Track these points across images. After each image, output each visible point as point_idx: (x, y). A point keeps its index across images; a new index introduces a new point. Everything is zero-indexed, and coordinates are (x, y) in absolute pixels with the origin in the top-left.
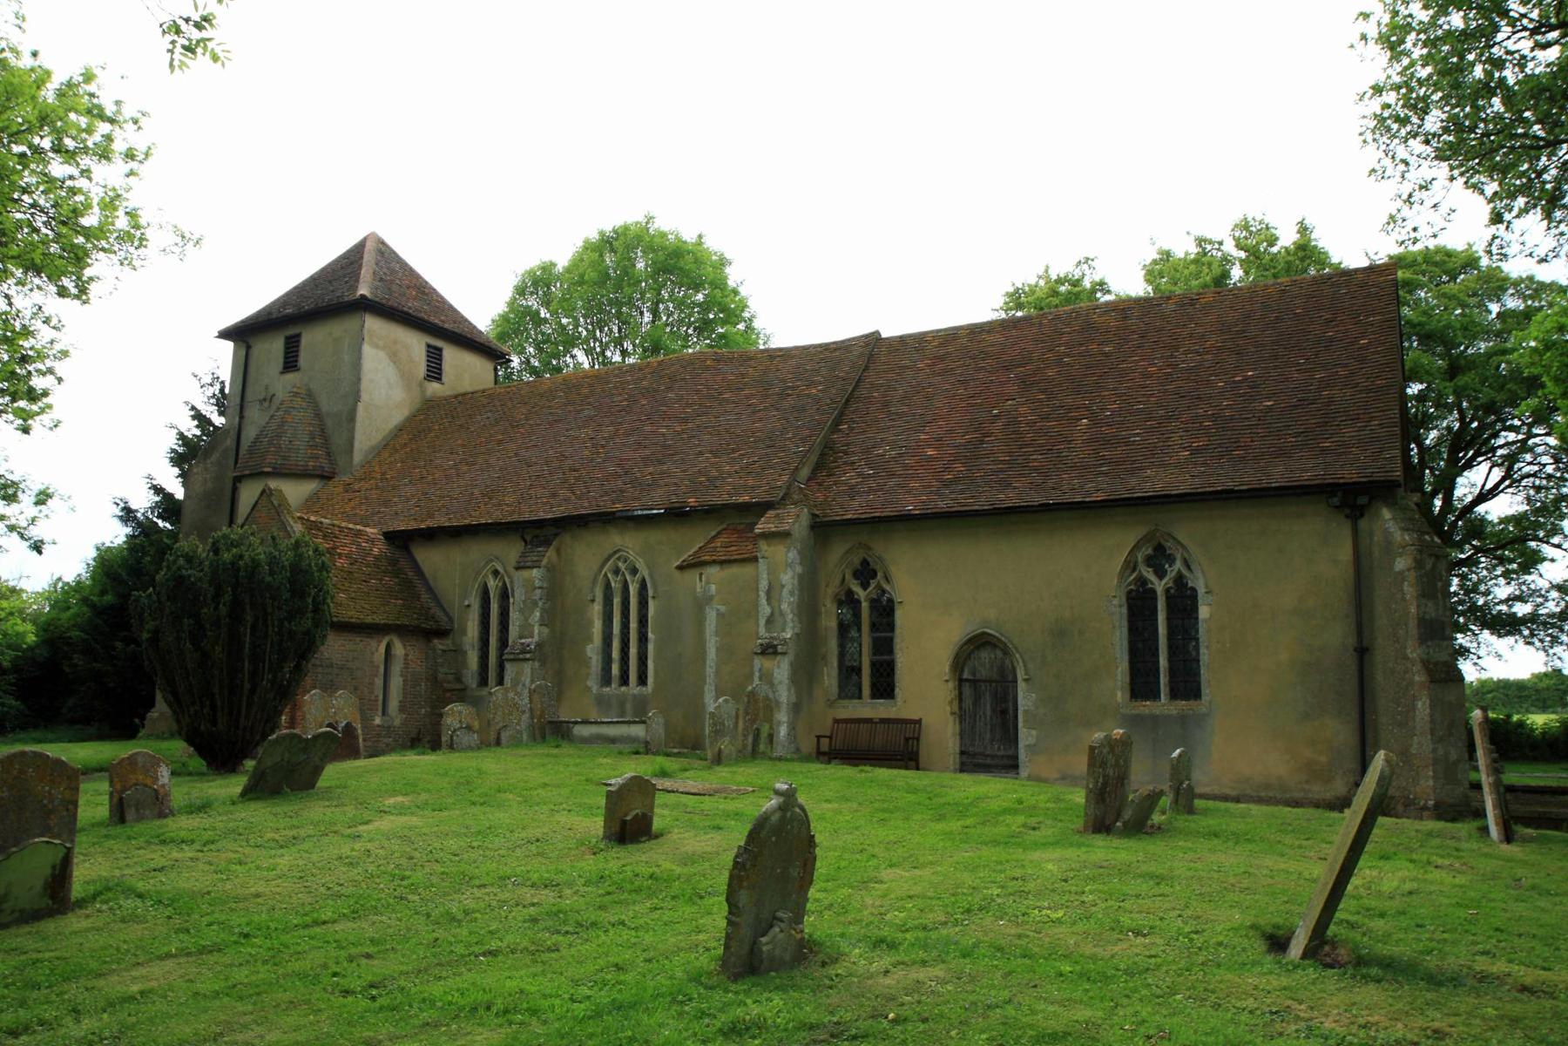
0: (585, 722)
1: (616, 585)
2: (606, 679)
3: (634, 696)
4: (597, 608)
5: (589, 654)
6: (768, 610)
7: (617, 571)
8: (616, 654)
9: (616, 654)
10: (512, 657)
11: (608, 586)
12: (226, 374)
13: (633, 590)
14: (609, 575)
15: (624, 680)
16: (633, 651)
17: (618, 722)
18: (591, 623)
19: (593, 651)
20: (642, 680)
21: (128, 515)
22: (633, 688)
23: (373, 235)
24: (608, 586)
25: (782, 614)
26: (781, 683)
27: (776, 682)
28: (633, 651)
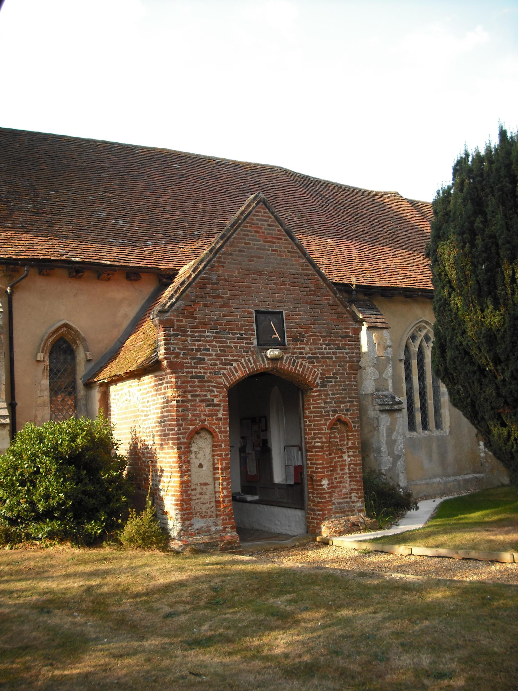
1: (414, 349)
2: (412, 426)
3: (437, 437)
8: (417, 404)
9: (417, 404)
15: (425, 426)
20: (438, 425)
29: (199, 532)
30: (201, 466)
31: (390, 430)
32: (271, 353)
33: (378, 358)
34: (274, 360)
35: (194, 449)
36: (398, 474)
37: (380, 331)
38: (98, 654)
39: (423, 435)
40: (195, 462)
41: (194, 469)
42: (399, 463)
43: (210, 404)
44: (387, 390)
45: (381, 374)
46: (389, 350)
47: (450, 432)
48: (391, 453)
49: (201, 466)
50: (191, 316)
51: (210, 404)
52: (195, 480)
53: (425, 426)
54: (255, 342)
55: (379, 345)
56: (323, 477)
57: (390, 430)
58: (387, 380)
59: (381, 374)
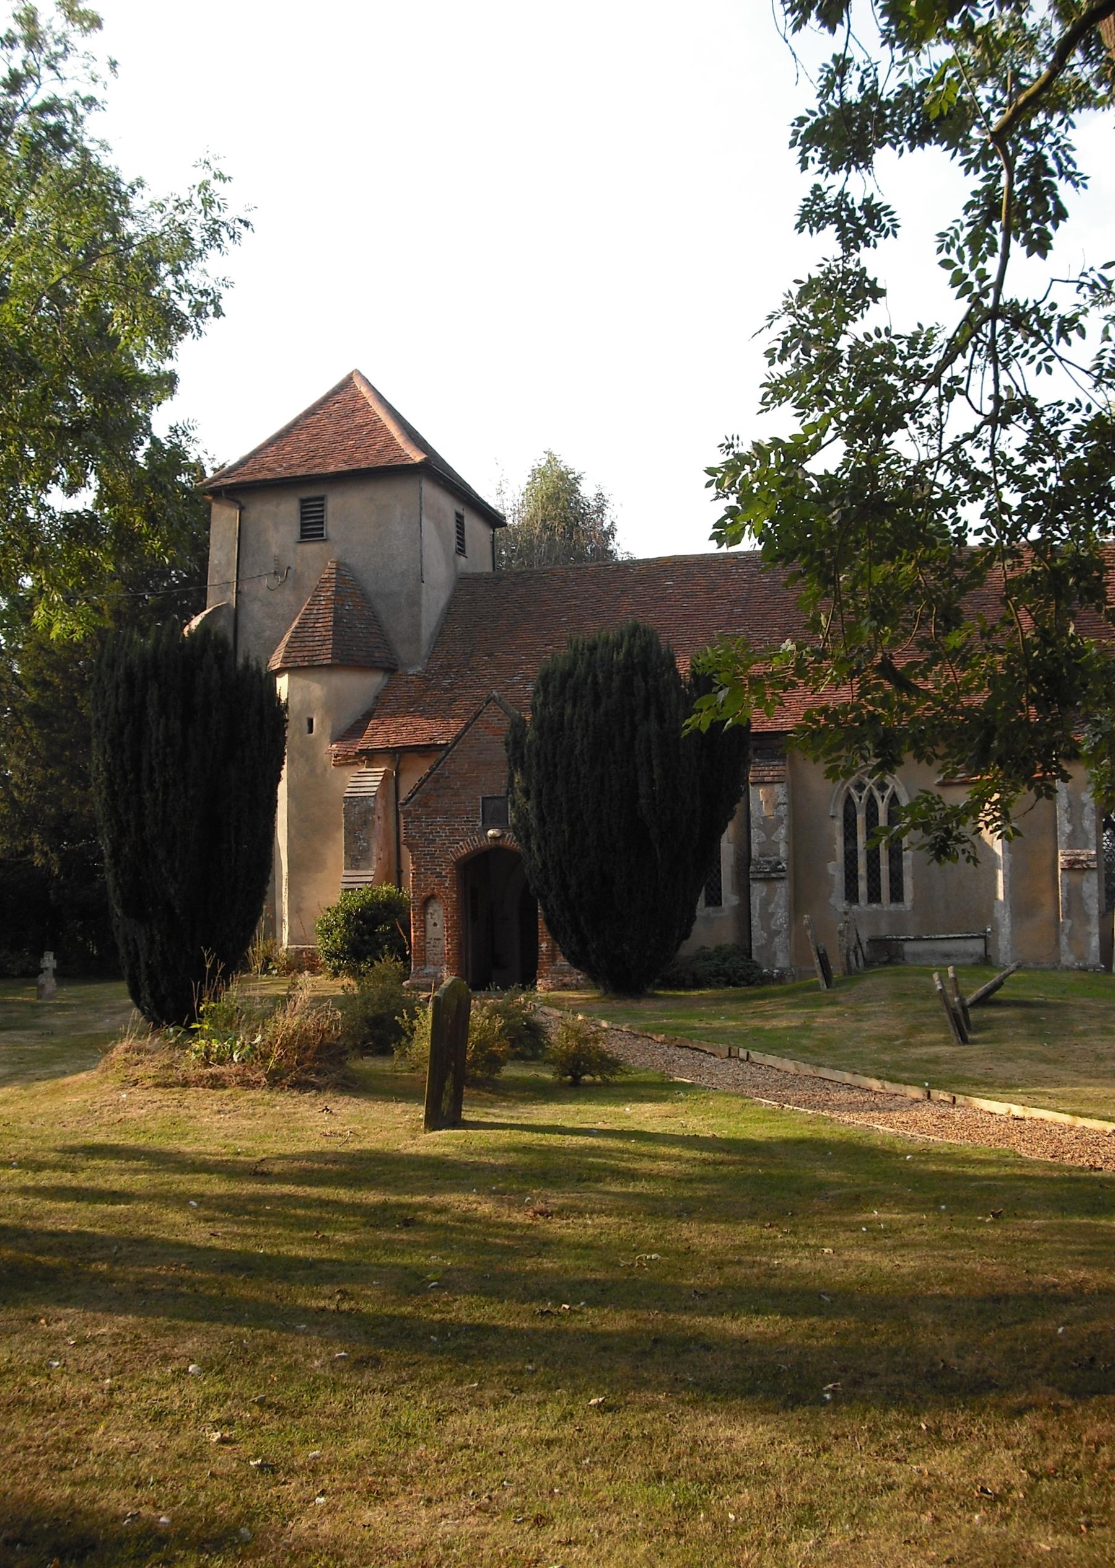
0: (918, 939)
1: (860, 803)
2: (851, 895)
3: (889, 913)
4: (839, 824)
5: (831, 871)
6: (1068, 828)
7: (860, 787)
8: (862, 871)
9: (862, 871)
10: (759, 876)
11: (849, 800)
12: (230, 464)
13: (882, 807)
14: (852, 790)
15: (874, 896)
16: (884, 868)
17: (959, 938)
18: (833, 840)
19: (835, 869)
20: (897, 895)
21: (923, 147)
22: (886, 904)
23: (356, 370)
24: (849, 800)
25: (1084, 831)
26: (1091, 896)
27: (1085, 895)
28: (884, 868)
29: (428, 975)
30: (435, 924)
31: (766, 902)
32: (491, 832)
33: (765, 818)
34: (493, 837)
35: (430, 911)
36: (775, 953)
37: (769, 788)
38: (593, 1195)
39: (867, 909)
40: (430, 921)
41: (430, 927)
42: (777, 940)
43: (439, 875)
44: (778, 854)
45: (768, 836)
46: (782, 808)
47: (913, 908)
48: (765, 927)
49: (435, 924)
50: (425, 805)
51: (439, 875)
52: (430, 935)
53: (874, 896)
54: (480, 824)
55: (767, 802)
56: (543, 941)
57: (766, 902)
58: (778, 843)
59: (768, 836)
